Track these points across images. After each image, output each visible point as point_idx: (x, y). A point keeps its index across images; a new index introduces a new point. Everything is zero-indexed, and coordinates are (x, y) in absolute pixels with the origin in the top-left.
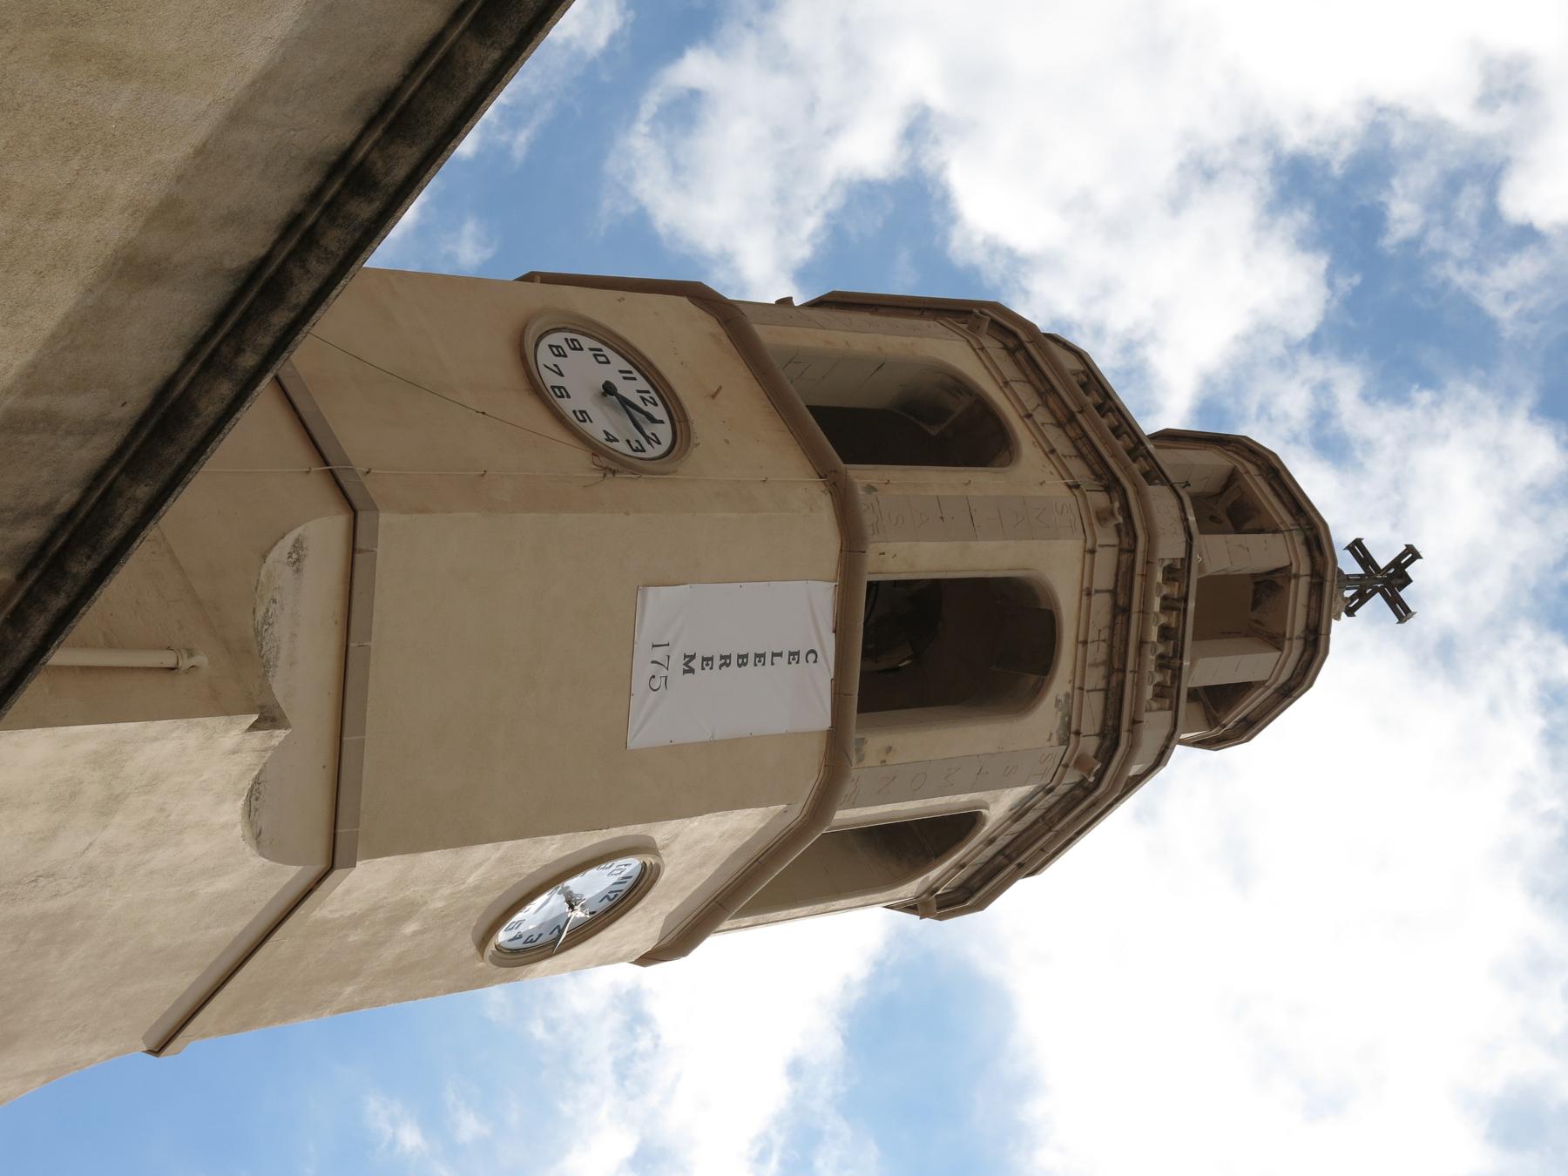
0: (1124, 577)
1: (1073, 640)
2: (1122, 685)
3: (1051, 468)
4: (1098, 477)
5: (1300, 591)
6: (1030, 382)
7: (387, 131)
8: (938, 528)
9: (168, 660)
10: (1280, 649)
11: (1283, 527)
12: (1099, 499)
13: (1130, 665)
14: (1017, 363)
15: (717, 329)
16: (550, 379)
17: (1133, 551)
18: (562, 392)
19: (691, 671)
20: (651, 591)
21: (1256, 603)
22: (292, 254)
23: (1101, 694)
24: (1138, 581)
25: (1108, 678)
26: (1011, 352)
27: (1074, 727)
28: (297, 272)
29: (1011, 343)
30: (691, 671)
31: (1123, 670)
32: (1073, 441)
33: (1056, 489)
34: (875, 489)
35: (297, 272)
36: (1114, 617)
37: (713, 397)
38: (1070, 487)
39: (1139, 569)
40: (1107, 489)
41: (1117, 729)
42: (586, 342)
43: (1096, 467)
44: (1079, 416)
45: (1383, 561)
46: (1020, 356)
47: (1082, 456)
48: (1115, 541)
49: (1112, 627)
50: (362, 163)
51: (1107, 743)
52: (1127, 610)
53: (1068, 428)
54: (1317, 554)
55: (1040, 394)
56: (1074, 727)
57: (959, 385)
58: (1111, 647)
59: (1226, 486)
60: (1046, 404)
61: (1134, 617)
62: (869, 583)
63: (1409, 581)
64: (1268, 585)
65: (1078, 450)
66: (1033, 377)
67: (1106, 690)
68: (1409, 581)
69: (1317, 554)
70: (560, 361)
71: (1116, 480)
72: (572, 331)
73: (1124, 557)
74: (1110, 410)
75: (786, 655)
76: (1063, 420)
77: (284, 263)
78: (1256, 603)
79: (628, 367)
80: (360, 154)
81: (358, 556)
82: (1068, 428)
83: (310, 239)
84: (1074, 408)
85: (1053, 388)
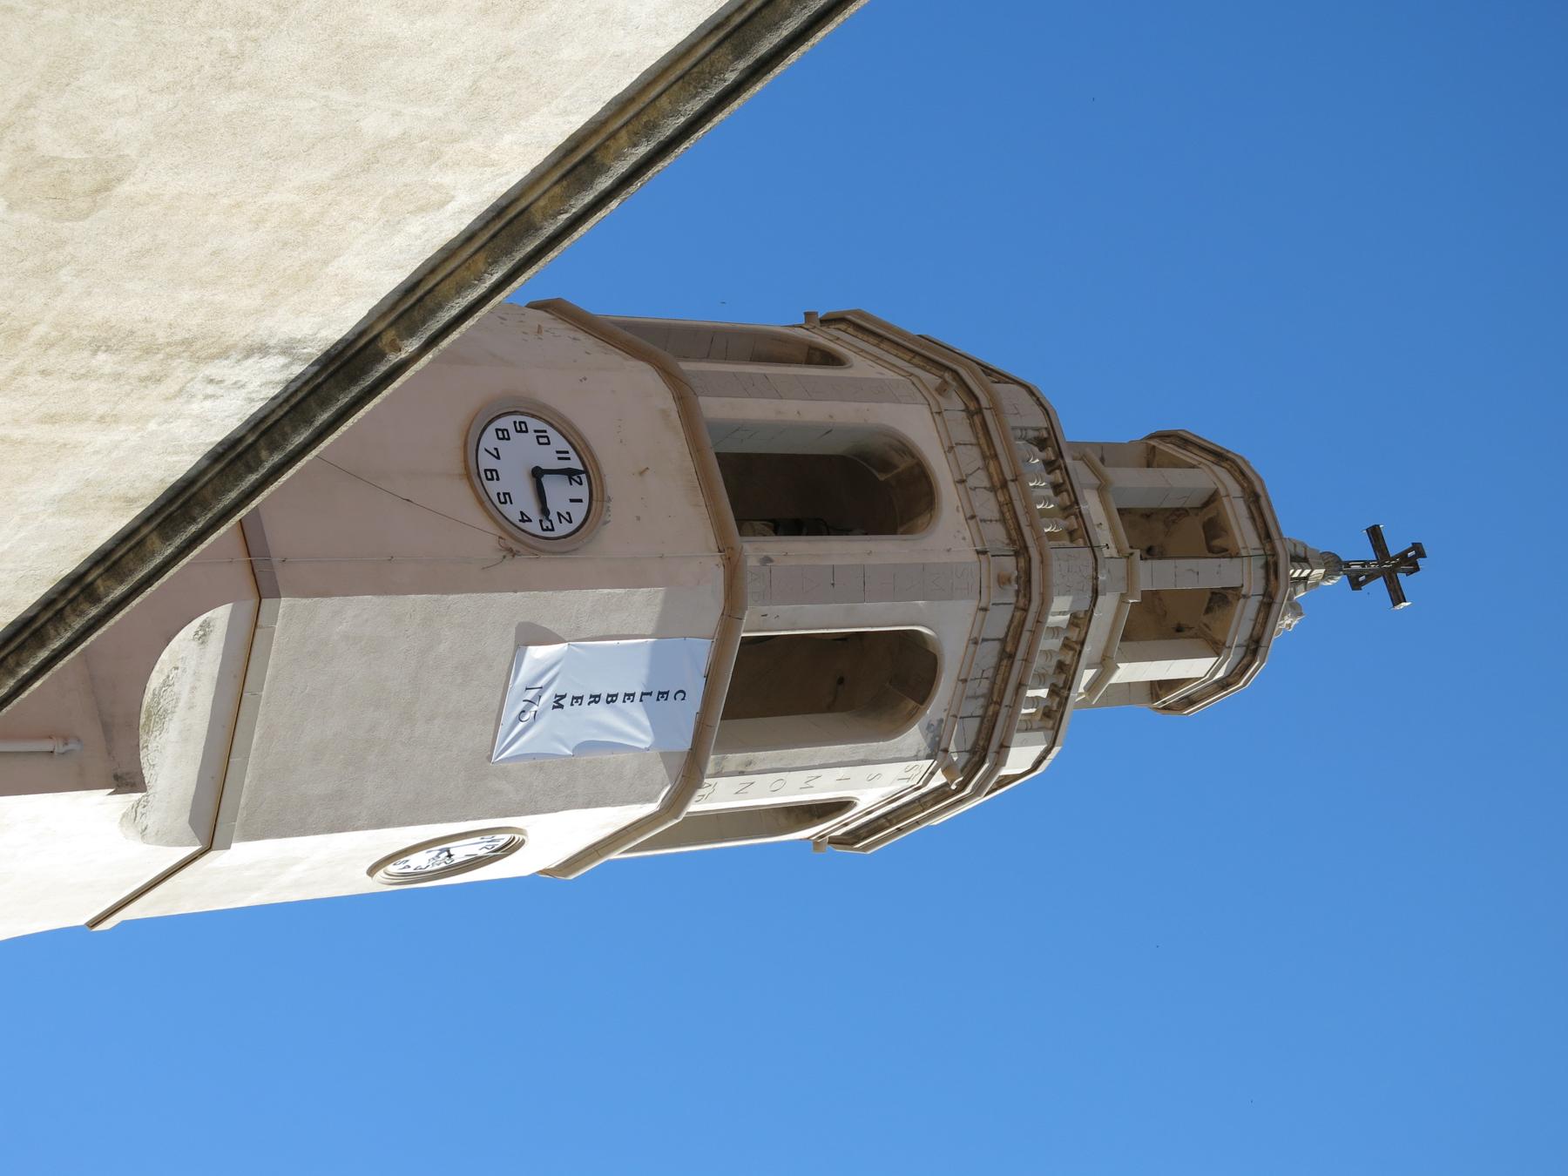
0: (1015, 630)
1: (954, 677)
2: (996, 714)
3: (967, 535)
4: (1012, 541)
5: (1250, 608)
6: (979, 445)
7: (107, 570)
8: (826, 588)
9: (47, 746)
10: (1218, 655)
11: (1243, 553)
12: (1009, 565)
13: (1006, 701)
14: (972, 425)
15: (671, 405)
16: (486, 462)
17: (1025, 610)
18: (493, 474)
19: (561, 706)
20: (531, 649)
21: (1208, 610)
22: (49, 620)
23: (978, 720)
24: (1026, 636)
25: (986, 708)
26: (970, 414)
27: (943, 746)
28: (52, 632)
29: (972, 406)
30: (561, 706)
31: (1000, 704)
32: (1000, 505)
33: (965, 554)
34: (770, 560)
35: (52, 632)
36: (1001, 660)
37: (642, 473)
38: (978, 552)
39: (1029, 624)
40: (1017, 554)
41: (986, 749)
42: (533, 424)
43: (1013, 533)
44: (1012, 486)
45: (1394, 549)
46: (977, 419)
47: (1003, 520)
48: (1013, 600)
49: (997, 668)
50: (92, 583)
51: (976, 759)
52: (1012, 656)
53: (999, 493)
54: (1272, 577)
55: (984, 457)
56: (943, 746)
57: (905, 448)
58: (993, 683)
59: (1206, 504)
60: (986, 468)
61: (1017, 664)
62: (746, 642)
63: (1417, 569)
64: (1220, 599)
65: (1002, 513)
66: (983, 441)
67: (983, 718)
68: (1417, 569)
69: (1272, 577)
70: (502, 445)
71: (1026, 548)
72: (522, 414)
73: (1018, 614)
74: (1059, 468)
75: (655, 695)
76: (998, 484)
77: (43, 625)
78: (1208, 610)
79: (567, 447)
80: (90, 578)
81: (258, 631)
82: (999, 493)
83: (59, 617)
84: (1009, 476)
85: (995, 456)
